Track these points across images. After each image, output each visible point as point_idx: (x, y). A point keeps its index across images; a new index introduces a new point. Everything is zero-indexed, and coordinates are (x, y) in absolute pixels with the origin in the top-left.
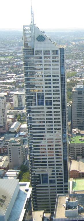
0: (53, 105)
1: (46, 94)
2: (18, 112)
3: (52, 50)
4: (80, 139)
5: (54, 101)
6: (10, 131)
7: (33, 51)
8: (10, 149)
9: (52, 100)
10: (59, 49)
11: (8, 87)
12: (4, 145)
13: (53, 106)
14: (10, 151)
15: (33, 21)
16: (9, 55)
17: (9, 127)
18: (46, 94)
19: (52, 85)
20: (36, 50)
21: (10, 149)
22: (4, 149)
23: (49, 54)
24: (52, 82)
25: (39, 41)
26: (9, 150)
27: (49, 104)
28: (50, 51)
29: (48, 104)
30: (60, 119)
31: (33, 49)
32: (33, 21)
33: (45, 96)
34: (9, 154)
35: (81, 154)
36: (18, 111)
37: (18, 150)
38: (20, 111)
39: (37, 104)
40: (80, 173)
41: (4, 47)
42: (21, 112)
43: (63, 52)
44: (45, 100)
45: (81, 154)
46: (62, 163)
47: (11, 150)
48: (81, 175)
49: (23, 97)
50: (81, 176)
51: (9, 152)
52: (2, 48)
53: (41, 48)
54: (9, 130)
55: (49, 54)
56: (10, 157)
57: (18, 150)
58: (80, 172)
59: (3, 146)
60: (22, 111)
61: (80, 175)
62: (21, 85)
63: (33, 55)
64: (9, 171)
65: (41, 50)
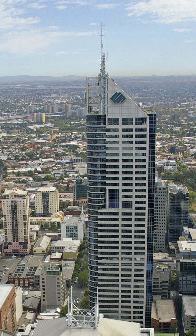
0: (134, 208)
1: (123, 191)
2: (45, 220)
3: (137, 117)
4: (158, 267)
5: (137, 202)
6: (35, 251)
7: (105, 120)
8: (43, 279)
9: (134, 200)
10: (148, 114)
11: (21, 180)
12: (28, 272)
13: (133, 211)
14: (43, 282)
15: (103, 70)
16: (15, 127)
17: (31, 244)
18: (123, 191)
19: (134, 176)
20: (109, 116)
21: (43, 279)
22: (28, 279)
23: (132, 123)
24: (134, 170)
25: (114, 102)
26: (41, 281)
27: (127, 208)
28: (118, 119)
29: (125, 208)
30: (144, 232)
31: (105, 116)
32: (103, 70)
33: (121, 194)
34: (42, 288)
35: (159, 292)
36: (44, 218)
37: (57, 281)
38: (47, 219)
39: (107, 206)
40: (160, 324)
41: (5, 115)
42: (49, 220)
43: (151, 121)
44: (121, 199)
45: (159, 292)
46: (144, 305)
47: (45, 281)
48: (162, 326)
49: (51, 197)
50: (162, 329)
51: (41, 284)
52: (2, 116)
53: (132, 114)
54: (34, 249)
55: (132, 123)
56: (44, 293)
57: (57, 281)
58: (160, 321)
59: (27, 275)
60: (50, 218)
61: (160, 327)
62: (43, 177)
63: (104, 126)
64: (41, 314)
65: (118, 117)
